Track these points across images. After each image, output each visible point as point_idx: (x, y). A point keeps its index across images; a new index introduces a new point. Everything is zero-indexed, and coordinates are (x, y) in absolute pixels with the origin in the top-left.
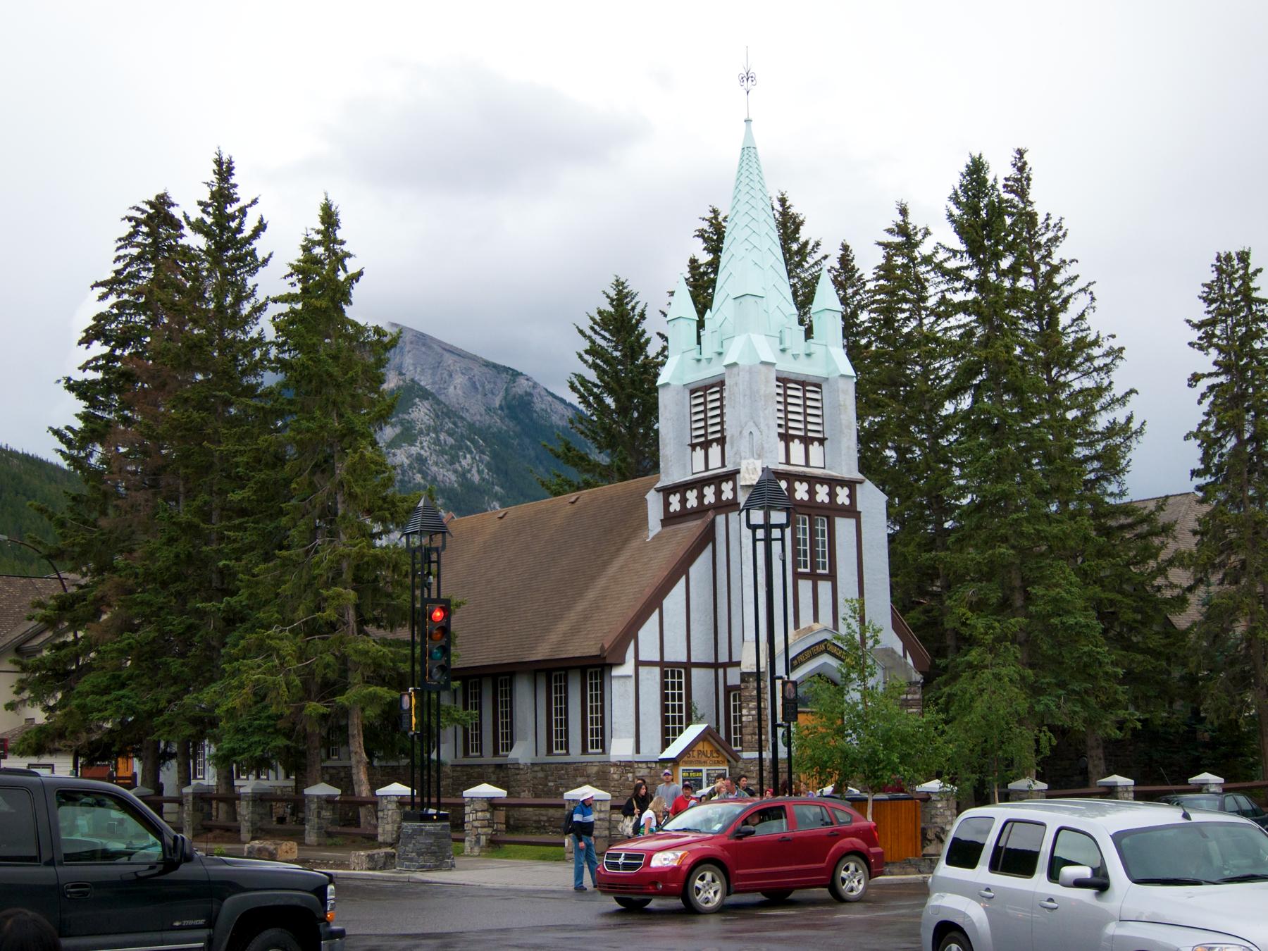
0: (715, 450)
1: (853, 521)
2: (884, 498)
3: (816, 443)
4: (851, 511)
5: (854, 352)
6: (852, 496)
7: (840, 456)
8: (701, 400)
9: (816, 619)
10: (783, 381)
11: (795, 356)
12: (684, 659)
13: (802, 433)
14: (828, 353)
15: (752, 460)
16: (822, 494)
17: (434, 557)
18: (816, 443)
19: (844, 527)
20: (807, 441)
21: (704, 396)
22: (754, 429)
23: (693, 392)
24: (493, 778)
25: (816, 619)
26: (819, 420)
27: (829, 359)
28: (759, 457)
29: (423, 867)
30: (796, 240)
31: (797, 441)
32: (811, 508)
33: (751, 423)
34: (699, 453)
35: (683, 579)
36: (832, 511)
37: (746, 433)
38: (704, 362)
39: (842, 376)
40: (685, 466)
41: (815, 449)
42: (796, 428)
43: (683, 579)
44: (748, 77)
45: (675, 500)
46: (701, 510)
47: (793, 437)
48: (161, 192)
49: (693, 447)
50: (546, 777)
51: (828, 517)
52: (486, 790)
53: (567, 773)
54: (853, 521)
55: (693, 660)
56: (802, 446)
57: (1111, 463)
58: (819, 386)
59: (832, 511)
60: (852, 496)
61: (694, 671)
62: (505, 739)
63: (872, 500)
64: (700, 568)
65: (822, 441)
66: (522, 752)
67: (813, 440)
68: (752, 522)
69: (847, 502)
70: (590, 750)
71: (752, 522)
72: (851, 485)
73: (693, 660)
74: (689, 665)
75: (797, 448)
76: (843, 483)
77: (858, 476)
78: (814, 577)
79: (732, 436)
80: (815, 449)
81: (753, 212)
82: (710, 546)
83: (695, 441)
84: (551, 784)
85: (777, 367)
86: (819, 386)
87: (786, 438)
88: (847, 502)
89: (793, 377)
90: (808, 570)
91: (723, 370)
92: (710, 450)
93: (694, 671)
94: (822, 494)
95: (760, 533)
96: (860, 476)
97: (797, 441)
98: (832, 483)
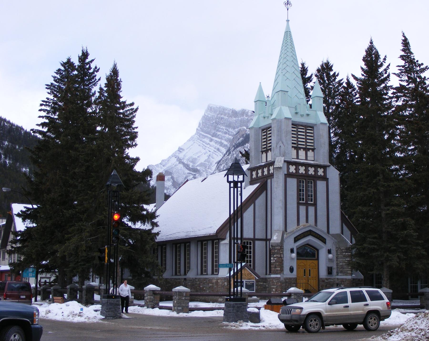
0: (269, 153)
1: (325, 182)
2: (338, 172)
3: (311, 151)
4: (325, 178)
5: (327, 114)
6: (325, 172)
7: (321, 156)
8: (265, 134)
9: (307, 221)
10: (295, 125)
11: (302, 116)
12: (252, 236)
13: (304, 147)
14: (316, 115)
15: (280, 157)
16: (311, 171)
17: (239, 185)
18: (311, 151)
19: (321, 185)
20: (306, 150)
21: (266, 132)
22: (281, 145)
23: (263, 130)
24: (183, 284)
25: (307, 221)
26: (312, 141)
27: (317, 116)
28: (284, 156)
29: (214, 322)
30: (332, 70)
31: (302, 150)
32: (306, 176)
33: (281, 142)
34: (264, 154)
35: (252, 206)
36: (316, 178)
37: (278, 146)
38: (266, 118)
39: (322, 123)
40: (259, 160)
41: (310, 153)
42: (302, 144)
43: (252, 206)
44: (288, 3)
45: (254, 173)
46: (263, 176)
47: (300, 148)
48: (325, 61)
49: (262, 152)
50: (200, 284)
51: (314, 180)
52: (152, 287)
53: (206, 282)
54: (325, 182)
55: (256, 237)
56: (304, 152)
57: (129, 146)
58: (270, 127)
59: (316, 178)
60: (325, 172)
61: (257, 242)
62: (187, 269)
63: (334, 174)
64: (260, 201)
65: (313, 150)
66: (192, 274)
67: (309, 149)
68: (229, 180)
69: (322, 174)
70: (215, 273)
71: (229, 180)
72: (325, 167)
73: (256, 237)
74: (254, 240)
75: (302, 153)
76: (321, 166)
77: (329, 164)
78: (307, 205)
79: (274, 148)
80: (310, 153)
81: (288, 58)
82: (265, 192)
83: (263, 150)
84: (201, 286)
85: (292, 120)
86: (313, 127)
87: (297, 149)
88: (322, 174)
89: (301, 124)
90: (304, 202)
91: (270, 122)
92: (268, 154)
93: (257, 242)
94: (311, 171)
95: (232, 185)
96: (330, 164)
97: (302, 150)
98: (316, 167)
